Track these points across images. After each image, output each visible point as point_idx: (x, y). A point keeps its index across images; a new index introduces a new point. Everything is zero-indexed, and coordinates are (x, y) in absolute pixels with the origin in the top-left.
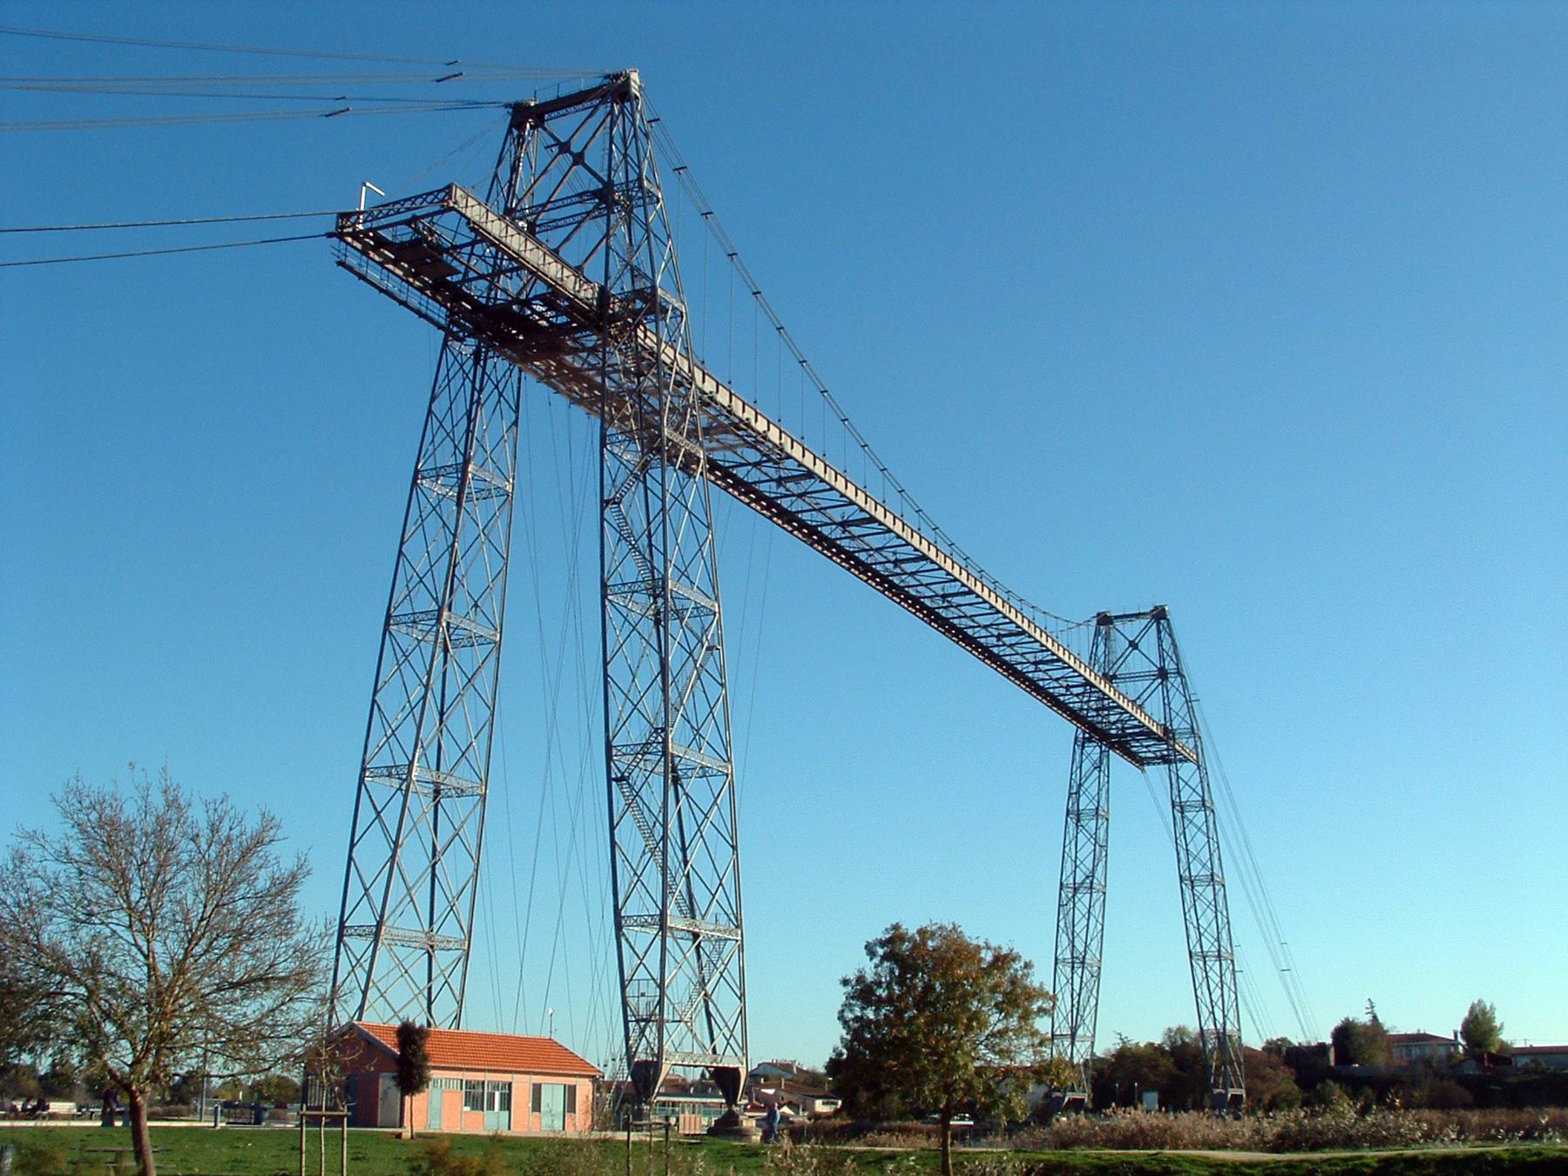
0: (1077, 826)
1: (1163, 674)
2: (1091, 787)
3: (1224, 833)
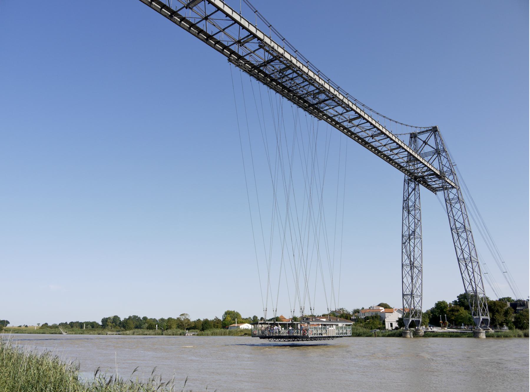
0: (408, 213)
1: (438, 152)
2: (412, 198)
3: (469, 211)
